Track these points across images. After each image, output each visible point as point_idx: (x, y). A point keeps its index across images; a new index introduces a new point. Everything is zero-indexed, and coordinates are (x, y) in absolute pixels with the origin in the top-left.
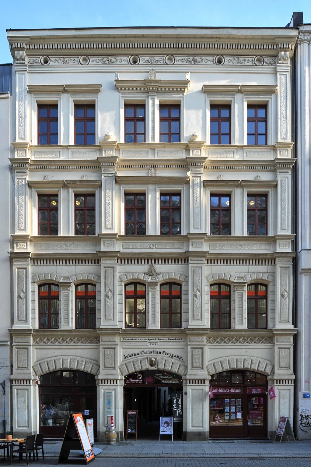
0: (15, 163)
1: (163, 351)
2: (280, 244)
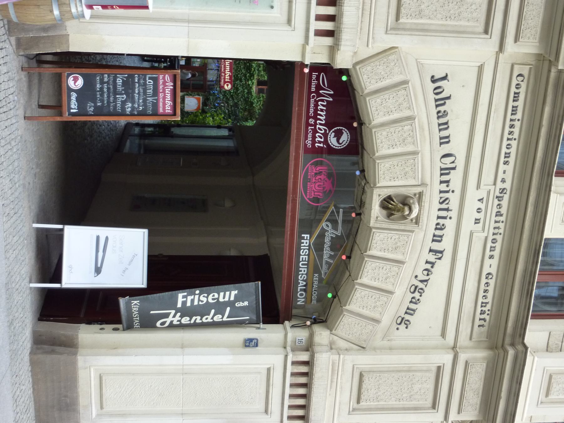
1: (441, 252)
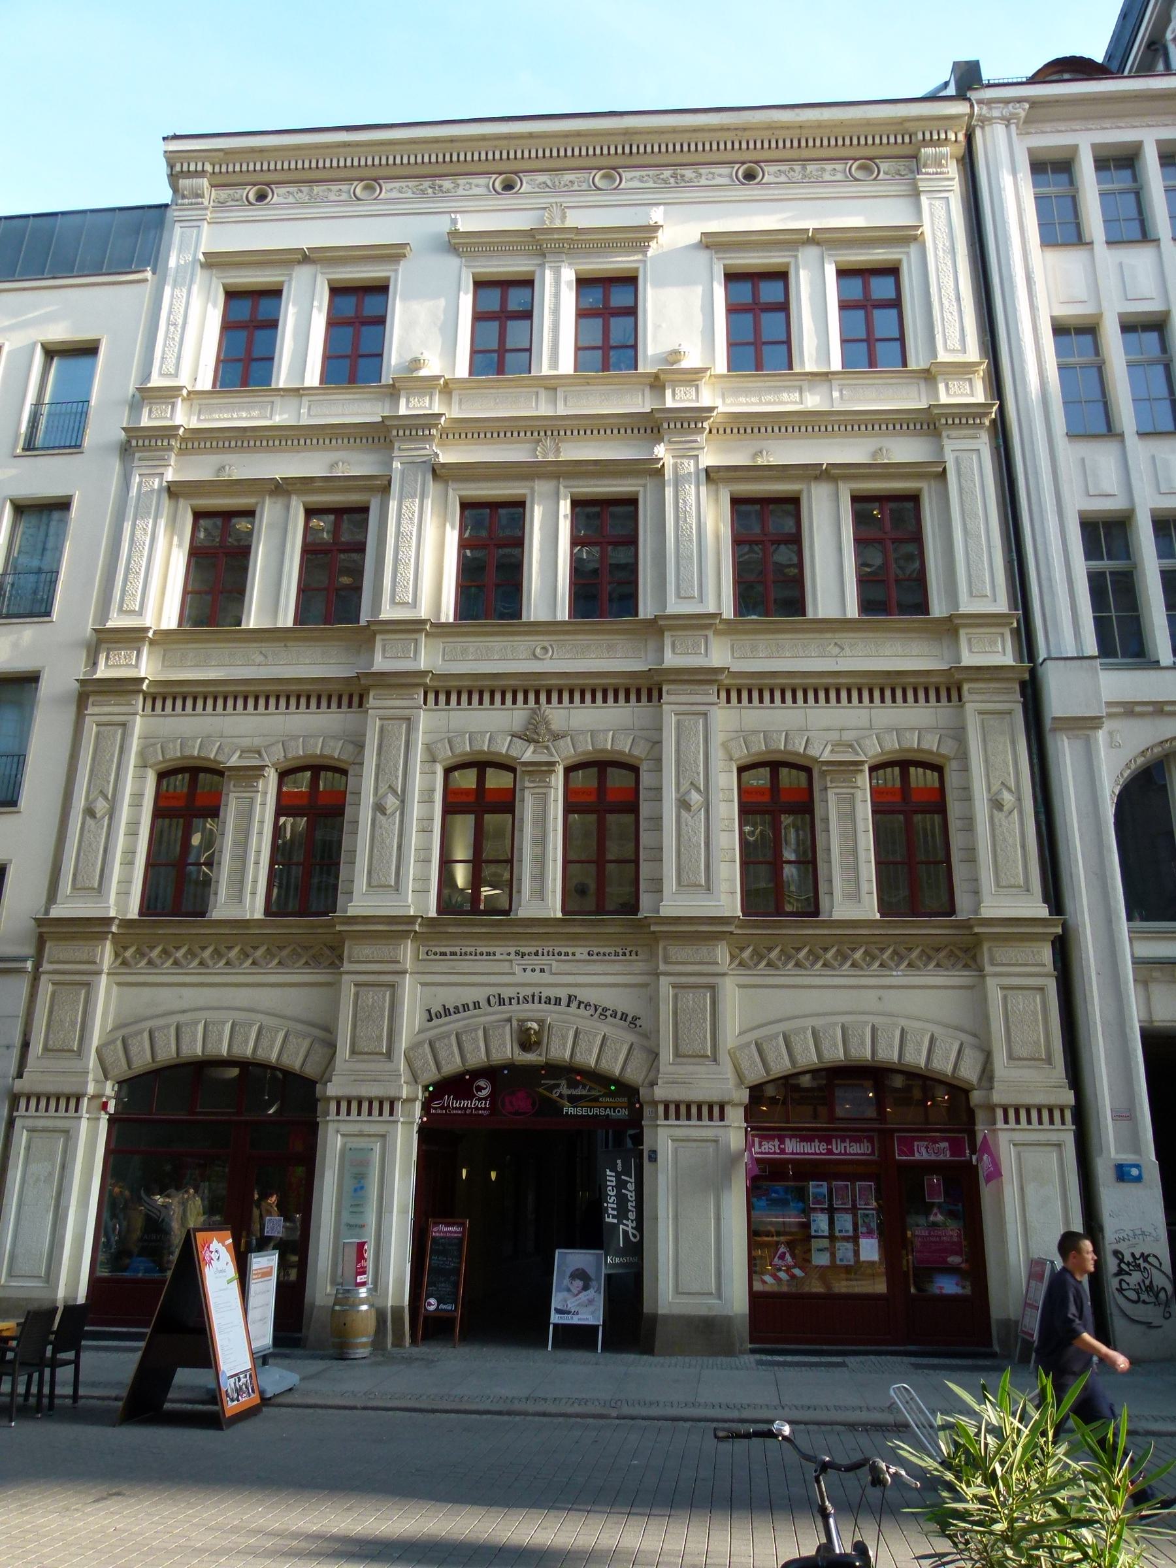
1: (570, 997)
2: (974, 642)
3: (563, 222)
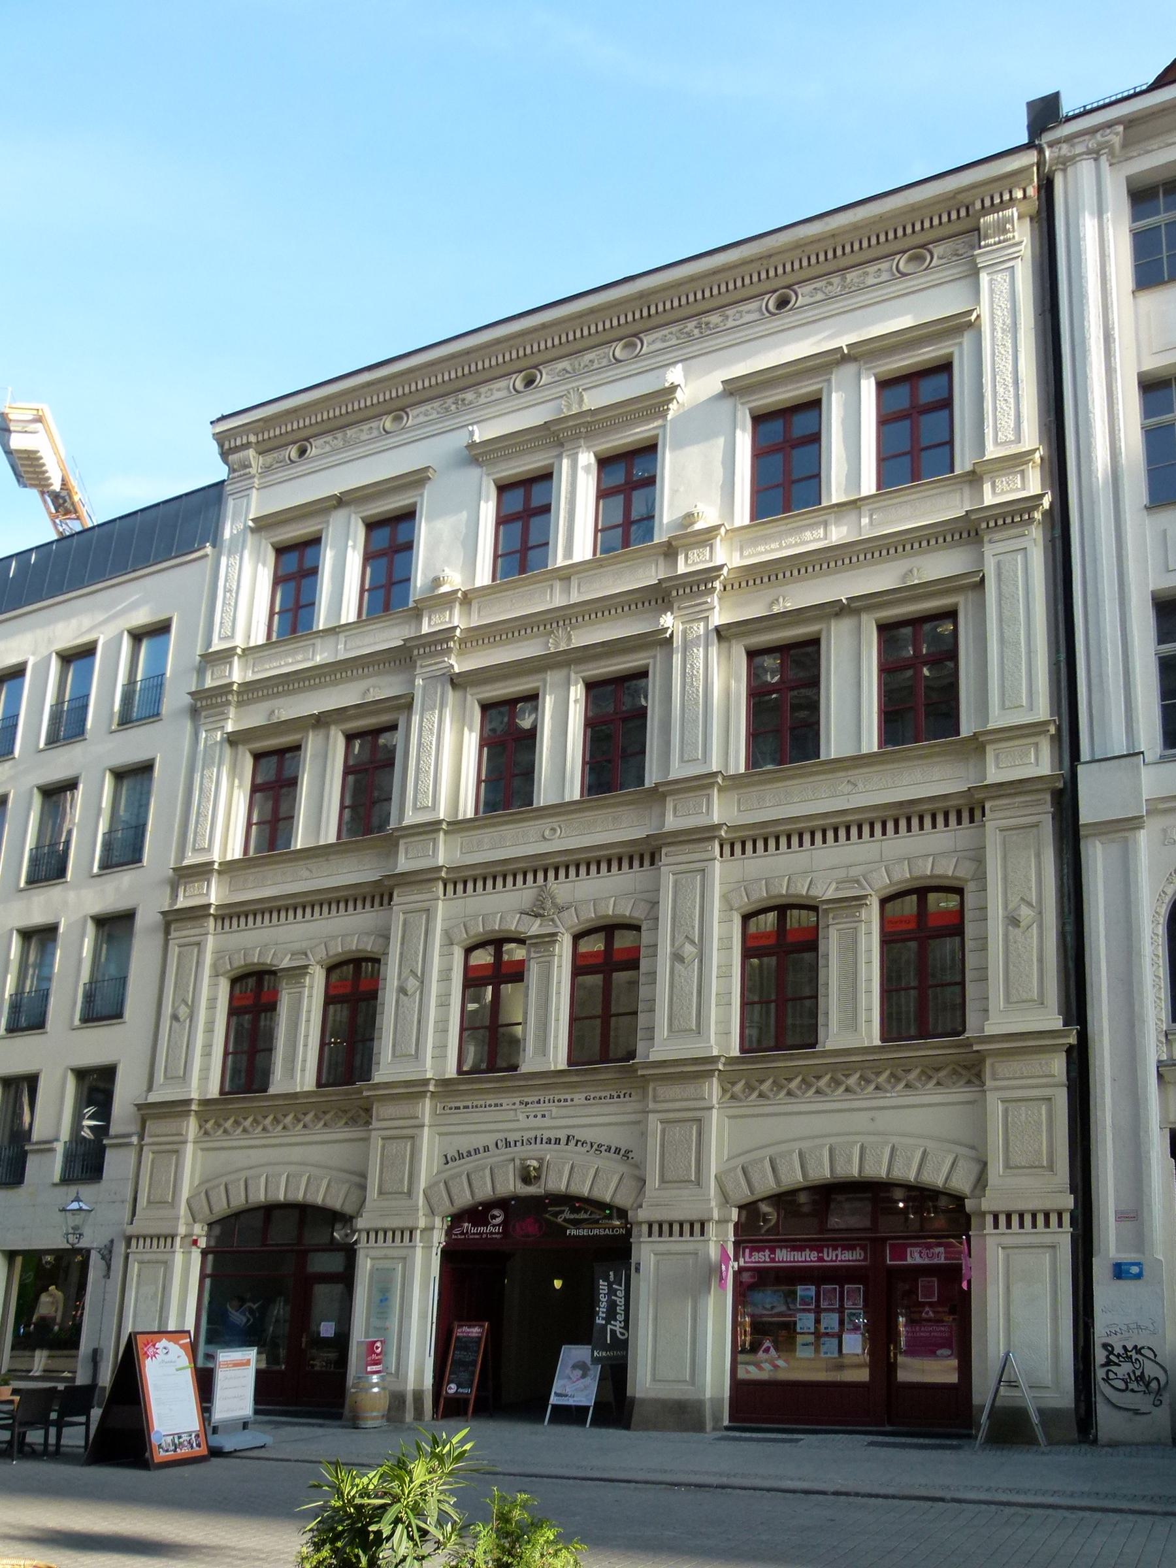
0: (201, 699)
1: (569, 1137)
2: (1002, 756)
3: (580, 406)
